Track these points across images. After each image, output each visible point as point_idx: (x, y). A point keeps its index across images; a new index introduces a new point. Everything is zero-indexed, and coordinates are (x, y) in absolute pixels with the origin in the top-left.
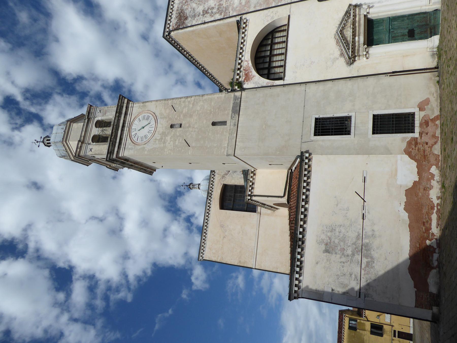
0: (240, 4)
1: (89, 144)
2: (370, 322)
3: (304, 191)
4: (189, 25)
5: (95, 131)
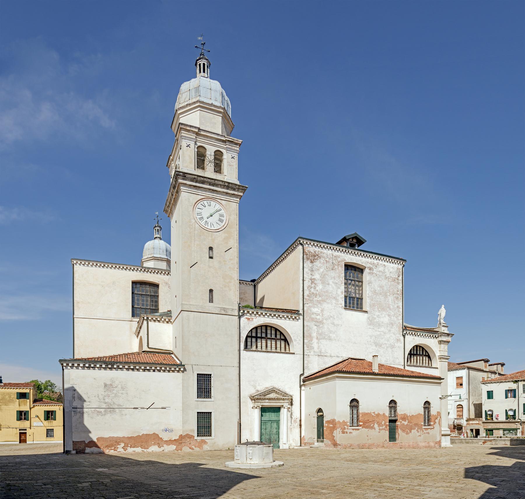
0: (313, 314)
1: (195, 142)
3: (153, 368)
5: (210, 151)
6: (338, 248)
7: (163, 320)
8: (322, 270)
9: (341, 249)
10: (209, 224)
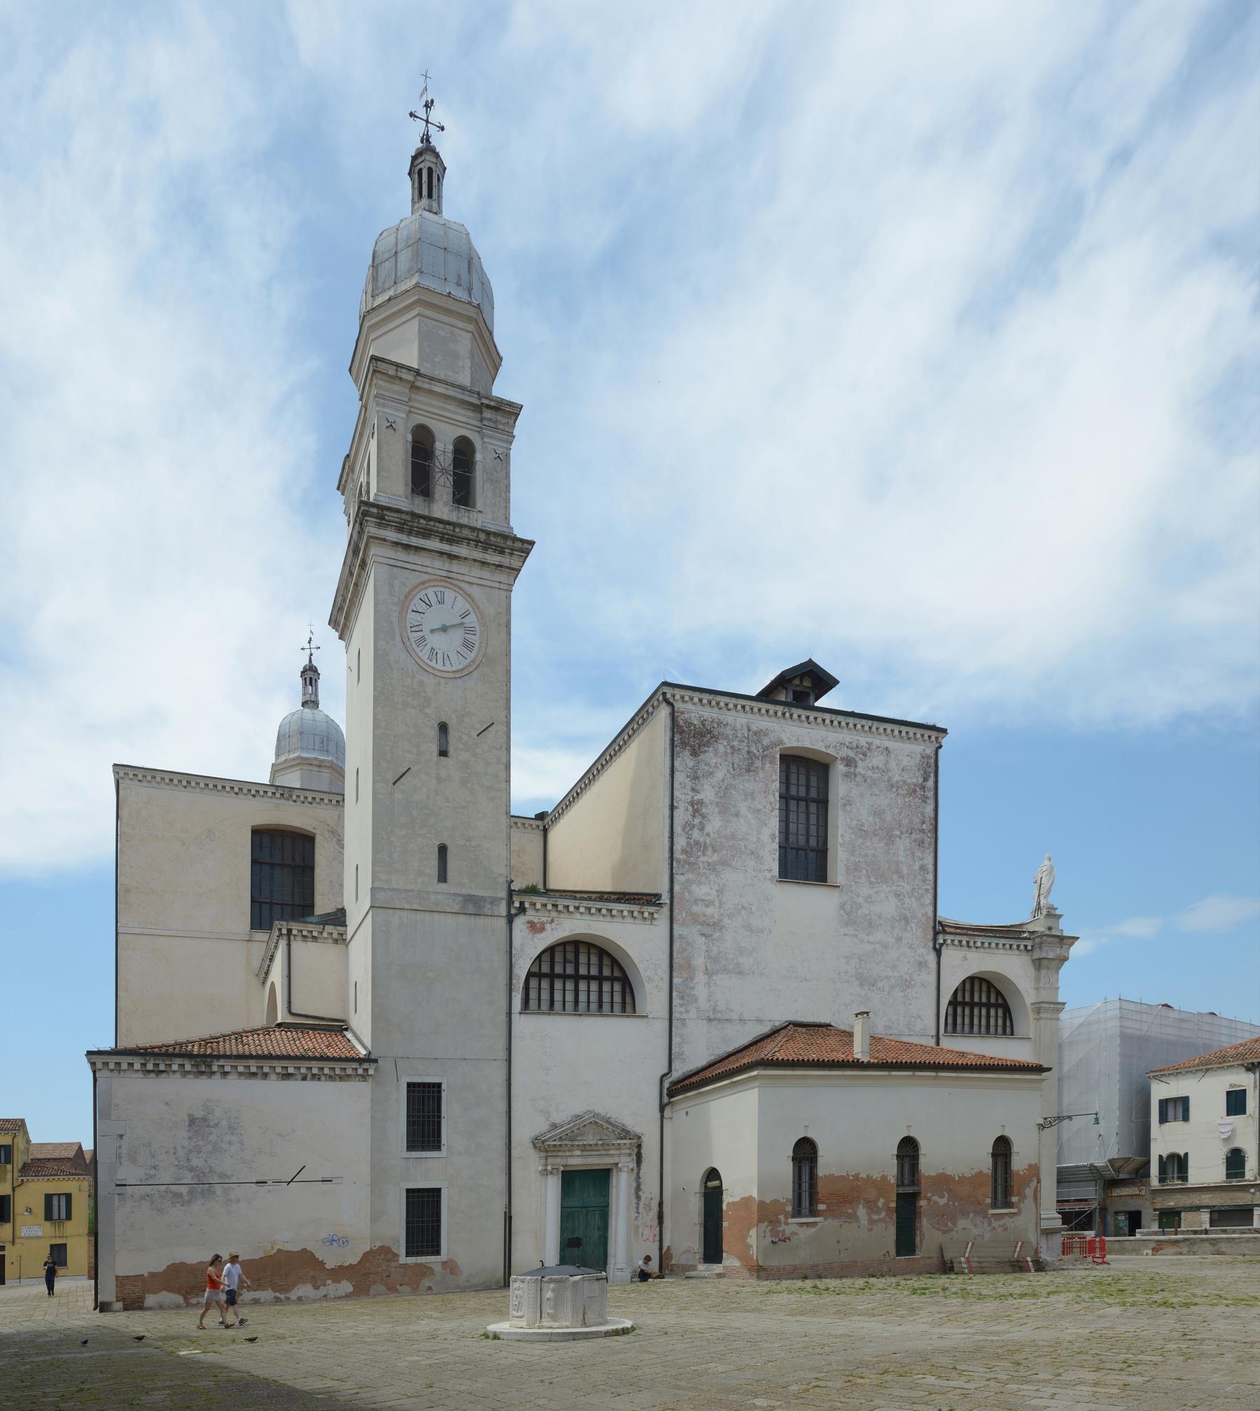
0: (696, 901)
2: (10, 1193)
4: (676, 763)
6: (764, 706)
7: (325, 935)
8: (720, 775)
9: (772, 708)
10: (440, 656)
